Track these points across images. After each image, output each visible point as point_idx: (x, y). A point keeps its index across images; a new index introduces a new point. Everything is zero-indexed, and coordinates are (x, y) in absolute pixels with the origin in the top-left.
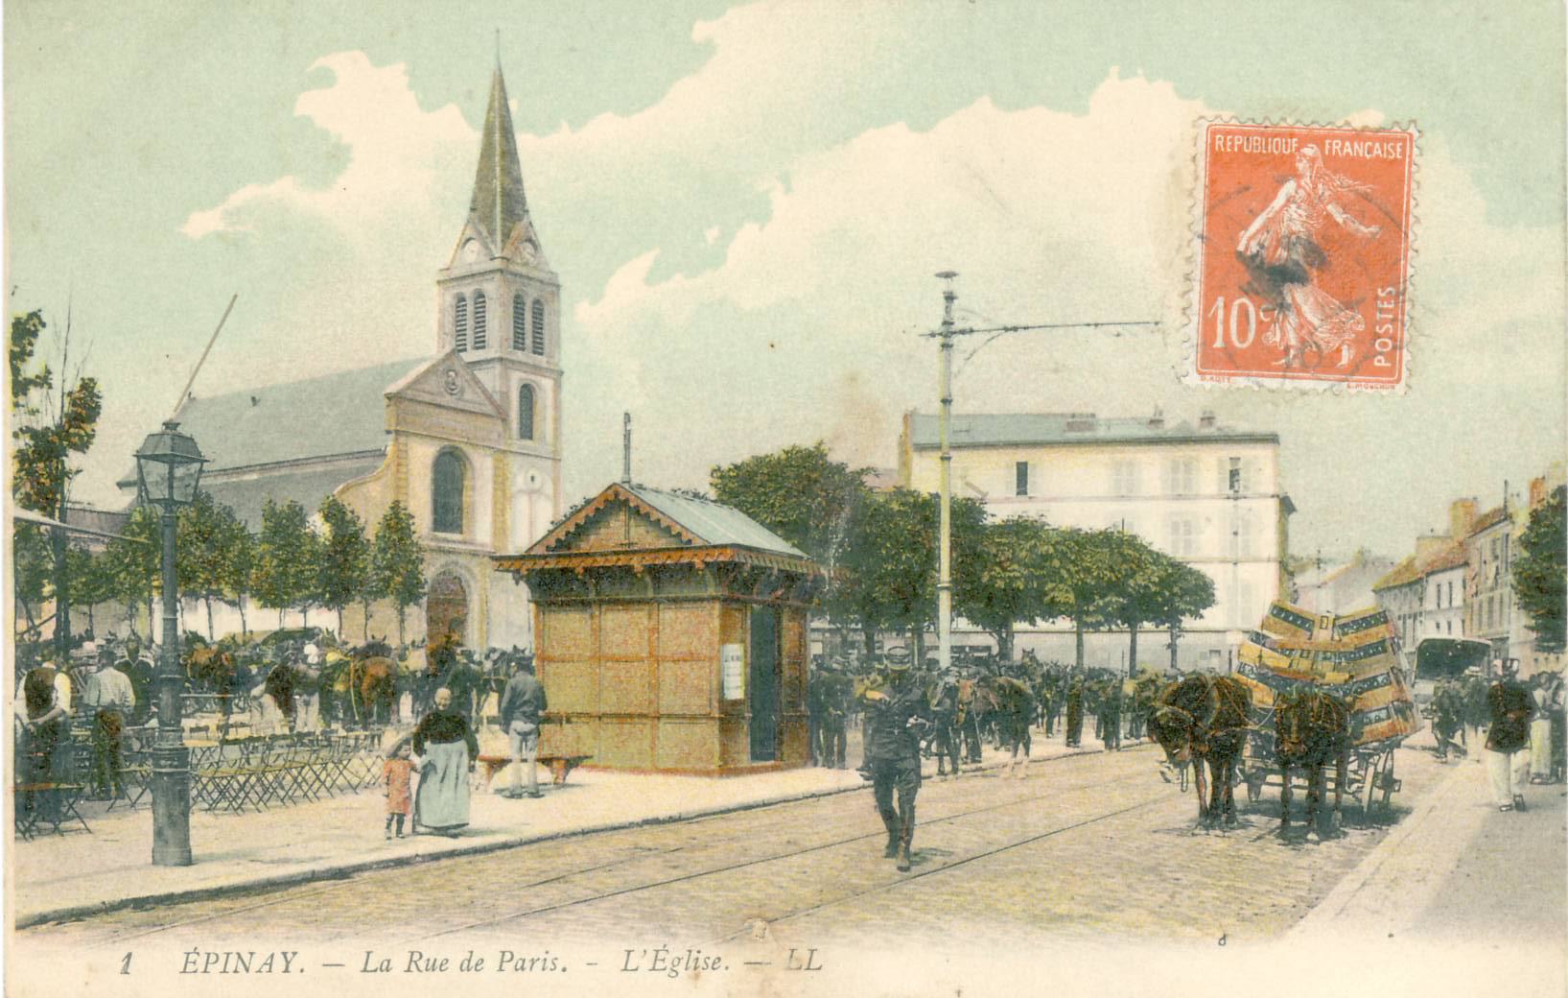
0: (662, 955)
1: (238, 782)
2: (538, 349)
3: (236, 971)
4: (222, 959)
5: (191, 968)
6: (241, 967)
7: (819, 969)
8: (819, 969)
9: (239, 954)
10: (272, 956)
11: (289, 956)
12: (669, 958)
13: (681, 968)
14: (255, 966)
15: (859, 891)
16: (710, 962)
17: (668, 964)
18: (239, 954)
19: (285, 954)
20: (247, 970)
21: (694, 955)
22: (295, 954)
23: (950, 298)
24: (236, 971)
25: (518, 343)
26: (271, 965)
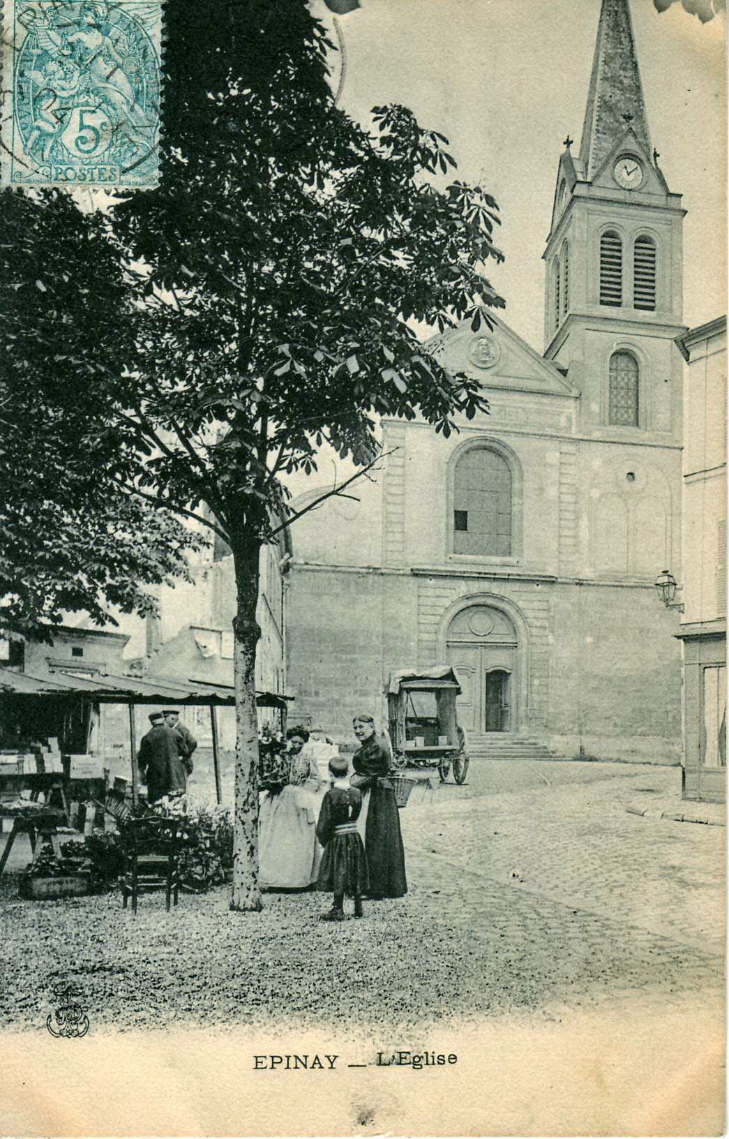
2: (645, 301)
25: (610, 296)
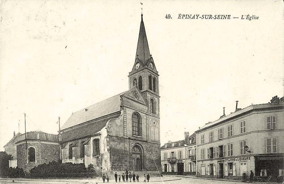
0: (248, 16)
1: (125, 123)
3: (188, 18)
4: (186, 16)
5: (180, 17)
6: (189, 18)
7: (244, 19)
8: (244, 19)
9: (188, 15)
10: (195, 15)
11: (198, 16)
12: (249, 17)
13: (251, 19)
14: (191, 18)
15: (221, 118)
16: (257, 18)
17: (249, 18)
18: (188, 15)
19: (197, 15)
20: (190, 18)
21: (254, 16)
22: (199, 15)
23: (42, 70)
24: (188, 18)
26: (194, 17)
